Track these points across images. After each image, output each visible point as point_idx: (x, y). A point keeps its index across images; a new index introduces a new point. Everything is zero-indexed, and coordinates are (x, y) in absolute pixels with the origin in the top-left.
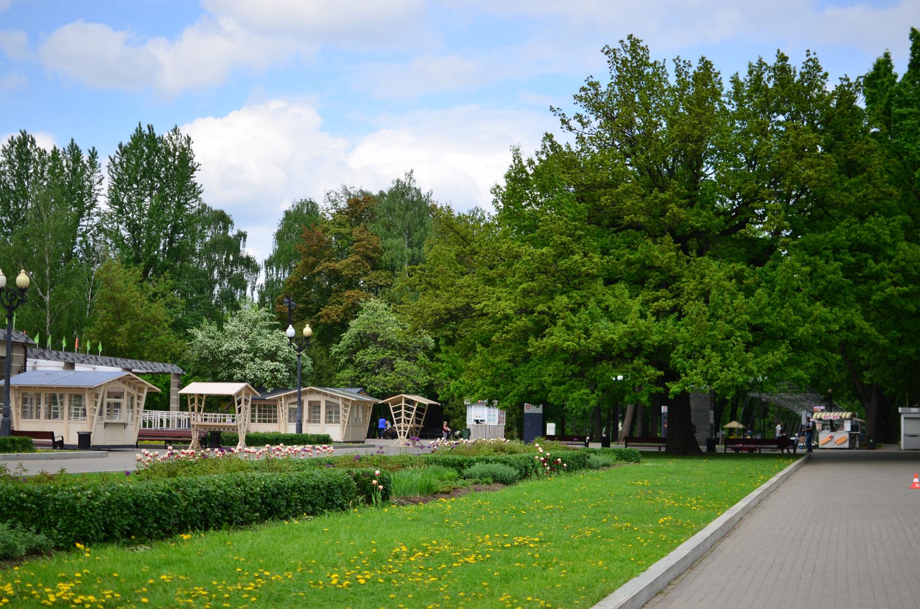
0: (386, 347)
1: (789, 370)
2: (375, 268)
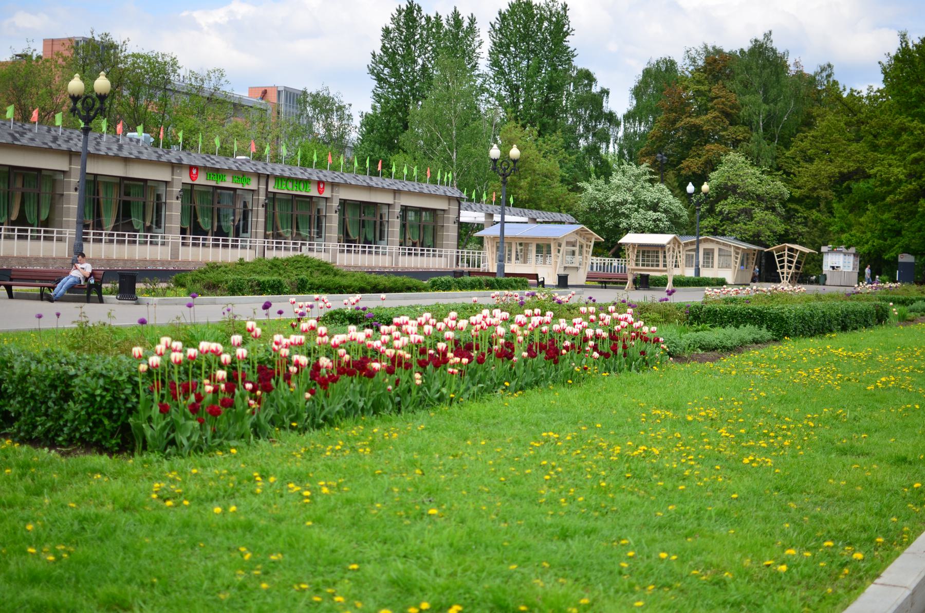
0: (744, 198)
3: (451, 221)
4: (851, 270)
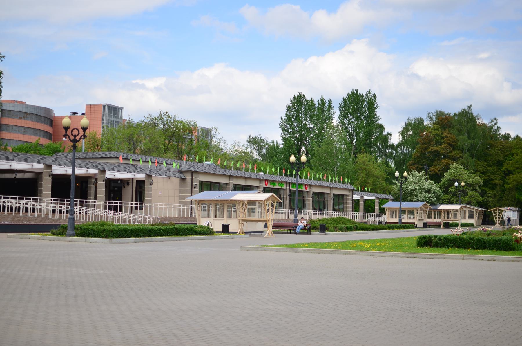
2: (454, 149)
3: (350, 200)
4: (516, 218)
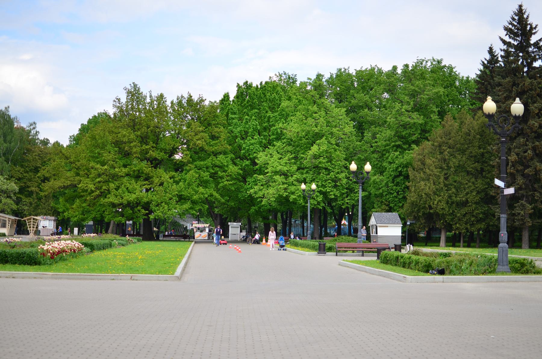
1: (190, 211)
4: (52, 228)
